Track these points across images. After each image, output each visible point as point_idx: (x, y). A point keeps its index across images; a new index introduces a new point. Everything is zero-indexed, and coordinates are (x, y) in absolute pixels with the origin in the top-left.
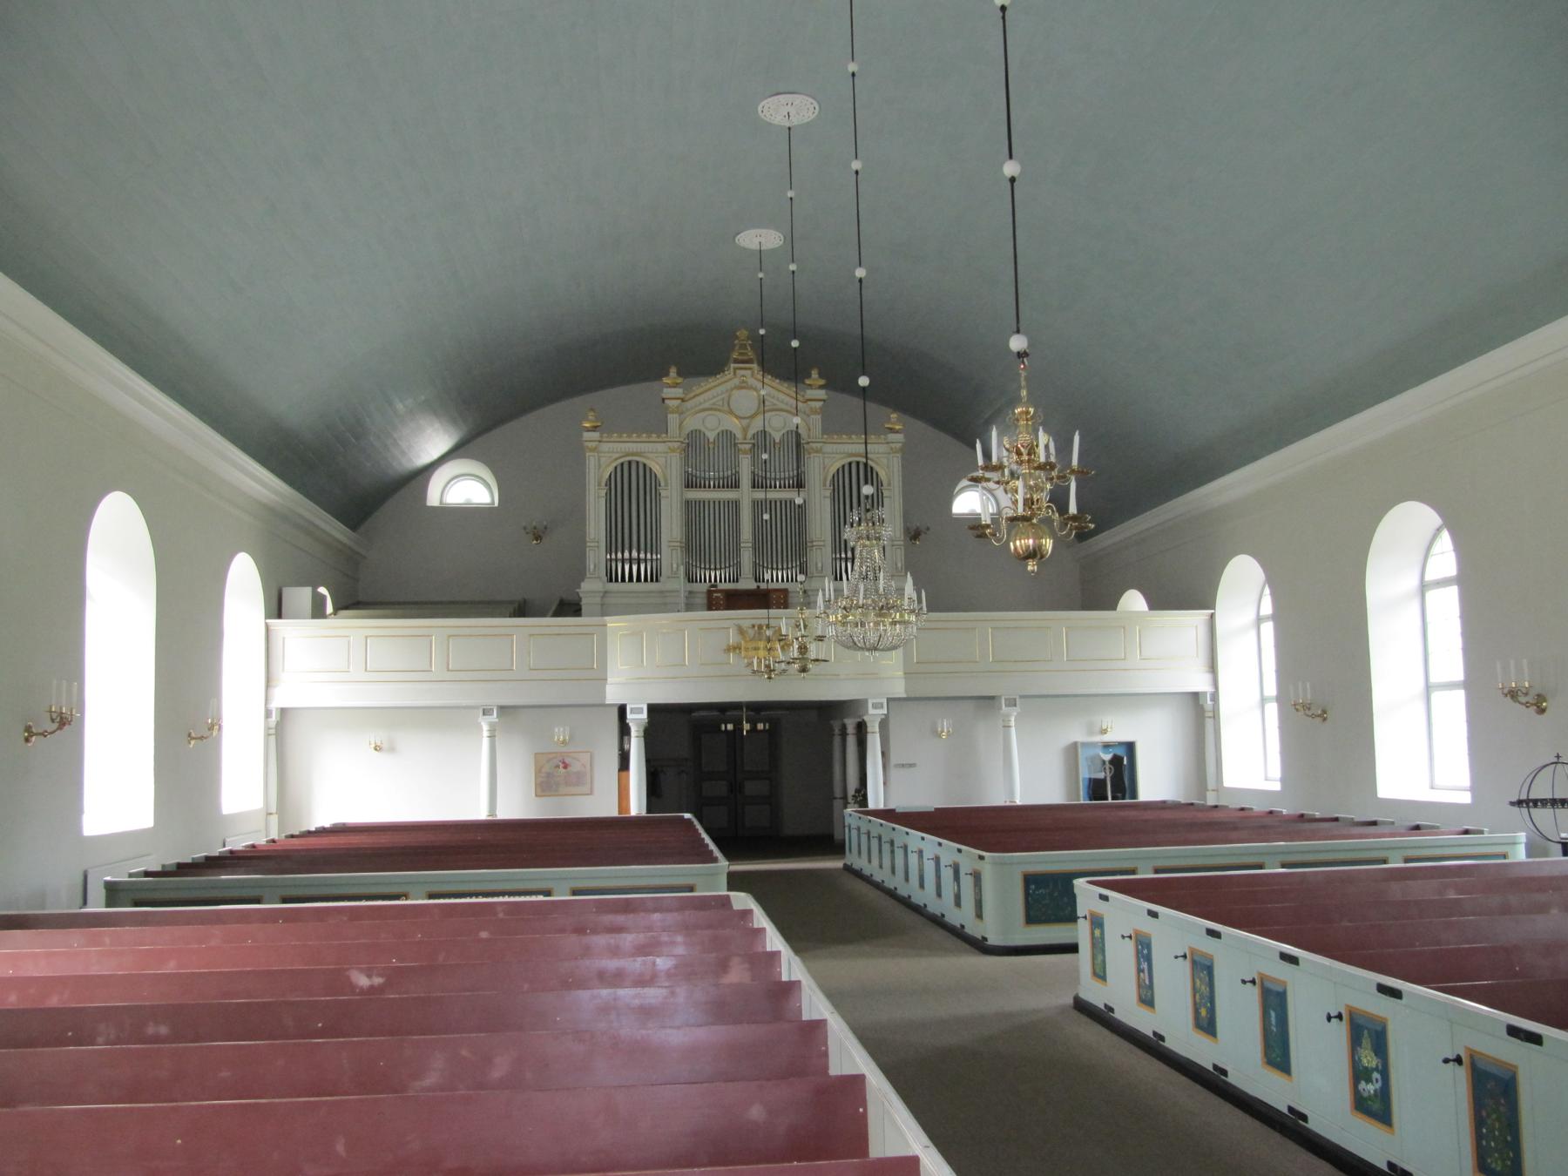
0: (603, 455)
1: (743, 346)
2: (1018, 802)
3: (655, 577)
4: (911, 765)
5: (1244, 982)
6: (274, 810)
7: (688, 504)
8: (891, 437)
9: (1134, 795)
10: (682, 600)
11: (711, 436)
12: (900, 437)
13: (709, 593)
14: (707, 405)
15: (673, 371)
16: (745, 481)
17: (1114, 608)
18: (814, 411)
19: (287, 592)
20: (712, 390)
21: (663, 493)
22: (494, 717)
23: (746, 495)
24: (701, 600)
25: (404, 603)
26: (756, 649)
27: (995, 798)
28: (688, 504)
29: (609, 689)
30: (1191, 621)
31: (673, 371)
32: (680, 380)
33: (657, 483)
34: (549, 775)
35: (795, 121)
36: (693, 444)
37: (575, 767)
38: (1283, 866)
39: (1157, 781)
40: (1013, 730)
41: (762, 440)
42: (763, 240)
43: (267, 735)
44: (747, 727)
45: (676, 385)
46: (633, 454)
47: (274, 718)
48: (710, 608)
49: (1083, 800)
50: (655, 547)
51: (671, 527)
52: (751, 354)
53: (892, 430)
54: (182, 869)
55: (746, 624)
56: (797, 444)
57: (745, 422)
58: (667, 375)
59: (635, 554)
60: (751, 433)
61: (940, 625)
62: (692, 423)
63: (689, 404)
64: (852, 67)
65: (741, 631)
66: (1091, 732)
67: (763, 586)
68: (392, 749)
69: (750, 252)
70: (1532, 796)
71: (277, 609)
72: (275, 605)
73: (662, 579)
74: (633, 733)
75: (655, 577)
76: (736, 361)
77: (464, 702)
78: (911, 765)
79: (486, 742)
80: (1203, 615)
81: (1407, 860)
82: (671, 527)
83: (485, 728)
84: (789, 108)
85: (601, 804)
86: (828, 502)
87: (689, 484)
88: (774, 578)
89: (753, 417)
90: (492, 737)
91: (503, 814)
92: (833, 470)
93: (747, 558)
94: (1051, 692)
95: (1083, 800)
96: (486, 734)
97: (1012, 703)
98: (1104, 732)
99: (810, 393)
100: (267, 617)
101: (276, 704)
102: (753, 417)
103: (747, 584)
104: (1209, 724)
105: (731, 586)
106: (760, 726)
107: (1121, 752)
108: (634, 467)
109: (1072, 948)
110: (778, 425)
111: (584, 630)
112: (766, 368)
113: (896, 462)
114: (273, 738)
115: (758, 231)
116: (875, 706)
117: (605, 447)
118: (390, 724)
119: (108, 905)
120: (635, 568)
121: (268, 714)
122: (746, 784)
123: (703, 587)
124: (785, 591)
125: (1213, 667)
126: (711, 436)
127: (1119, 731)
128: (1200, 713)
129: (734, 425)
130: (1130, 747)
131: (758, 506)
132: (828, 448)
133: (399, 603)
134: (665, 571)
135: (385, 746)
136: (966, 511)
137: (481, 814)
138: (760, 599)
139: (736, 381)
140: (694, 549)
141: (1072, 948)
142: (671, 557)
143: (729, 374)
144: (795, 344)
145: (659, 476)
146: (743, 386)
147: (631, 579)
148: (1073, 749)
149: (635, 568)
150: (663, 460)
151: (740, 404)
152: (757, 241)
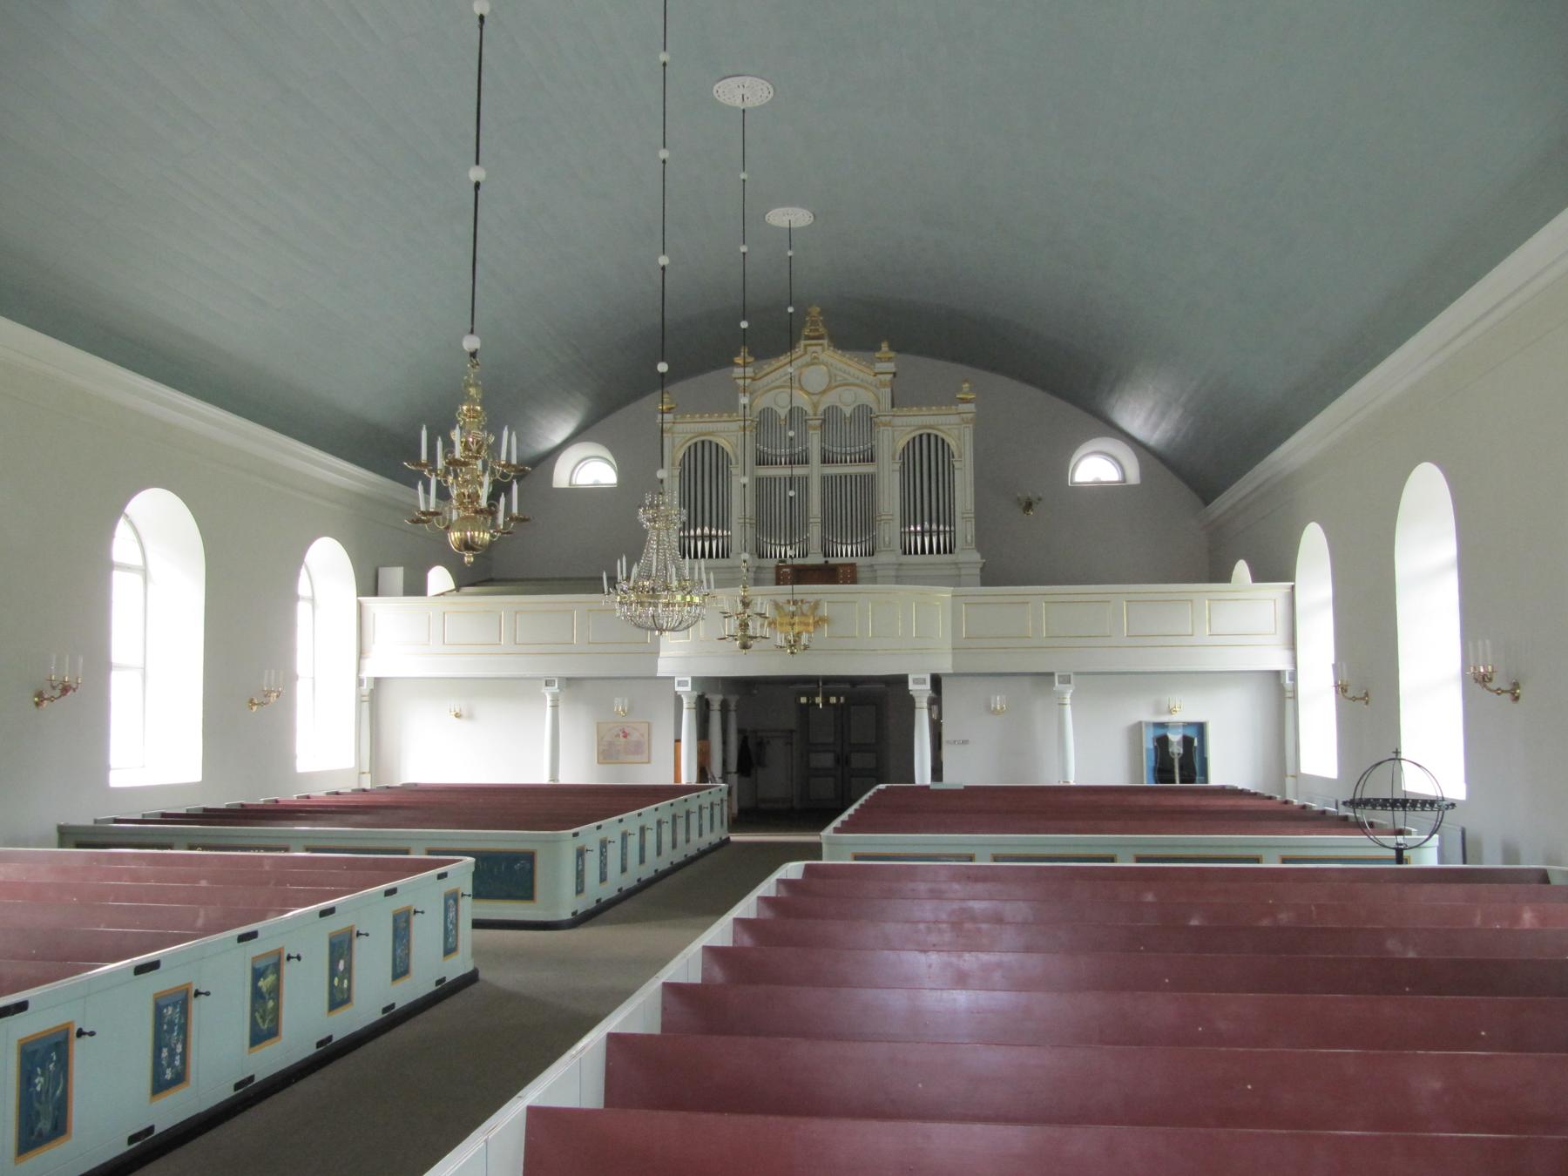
0: (682, 433)
1: (814, 323)
2: (1072, 781)
3: (725, 554)
4: (965, 742)
5: (299, 958)
6: (366, 768)
7: (759, 481)
8: (963, 407)
9: (1206, 781)
10: (773, 576)
11: (848, 411)
12: (971, 407)
13: (778, 568)
14: (778, 383)
15: (885, 346)
16: (815, 457)
17: (1254, 580)
18: (883, 384)
19: (383, 572)
20: (781, 369)
21: (957, 465)
22: (555, 689)
23: (815, 471)
24: (772, 575)
25: (522, 580)
26: (807, 624)
27: (1049, 778)
28: (759, 481)
29: (660, 662)
30: (1277, 590)
31: (885, 346)
32: (892, 354)
33: (951, 455)
34: (610, 744)
35: (749, 104)
36: (765, 422)
37: (634, 737)
38: (307, 850)
39: (1230, 765)
40: (1068, 709)
41: (830, 419)
42: (793, 218)
43: (360, 701)
44: (819, 700)
45: (889, 360)
46: (931, 427)
47: (366, 688)
48: (984, 583)
49: (1147, 781)
50: (724, 523)
51: (740, 504)
52: (822, 330)
53: (964, 401)
54: (167, 818)
55: (781, 599)
56: (866, 419)
57: (815, 398)
58: (738, 354)
59: (934, 527)
60: (821, 408)
61: (1080, 598)
62: (763, 402)
63: (760, 383)
64: (664, 57)
65: (777, 606)
66: (1158, 712)
67: (832, 561)
68: (471, 717)
69: (778, 229)
70: (1366, 795)
71: (370, 586)
72: (371, 583)
73: (957, 550)
74: (685, 705)
75: (725, 554)
76: (808, 338)
77: (528, 674)
78: (965, 742)
79: (549, 711)
80: (1283, 586)
81: (1284, 861)
82: (740, 504)
83: (549, 698)
84: (741, 91)
85: (657, 773)
86: (897, 476)
87: (760, 462)
88: (846, 553)
89: (824, 392)
90: (555, 706)
91: (566, 779)
92: (902, 443)
93: (815, 533)
94: (1090, 669)
95: (1147, 781)
96: (549, 703)
97: (1066, 680)
98: (1170, 712)
99: (880, 367)
100: (362, 592)
101: (371, 670)
102: (824, 392)
103: (816, 559)
104: (1289, 703)
105: (797, 561)
106: (833, 700)
107: (1191, 733)
108: (925, 438)
109: (478, 924)
110: (847, 400)
111: (1021, 599)
112: (842, 342)
113: (968, 434)
114: (366, 706)
115: (790, 210)
116: (916, 681)
117: (678, 427)
118: (469, 693)
119: (61, 846)
120: (927, 540)
121: (360, 682)
122: (808, 753)
123: (771, 563)
124: (853, 565)
125: (1293, 646)
126: (848, 411)
127: (1185, 709)
128: (1279, 691)
129: (802, 400)
130: (1201, 728)
131: (825, 479)
132: (897, 421)
133: (522, 580)
134: (736, 545)
135: (464, 713)
136: (1090, 479)
137: (543, 779)
138: (828, 574)
139: (807, 358)
140: (763, 523)
141: (478, 924)
142: (738, 532)
143: (799, 351)
144: (744, 325)
145: (731, 455)
146: (814, 362)
147: (923, 552)
148: (1136, 730)
149: (927, 540)
150: (728, 434)
151: (821, 378)
152: (786, 219)
